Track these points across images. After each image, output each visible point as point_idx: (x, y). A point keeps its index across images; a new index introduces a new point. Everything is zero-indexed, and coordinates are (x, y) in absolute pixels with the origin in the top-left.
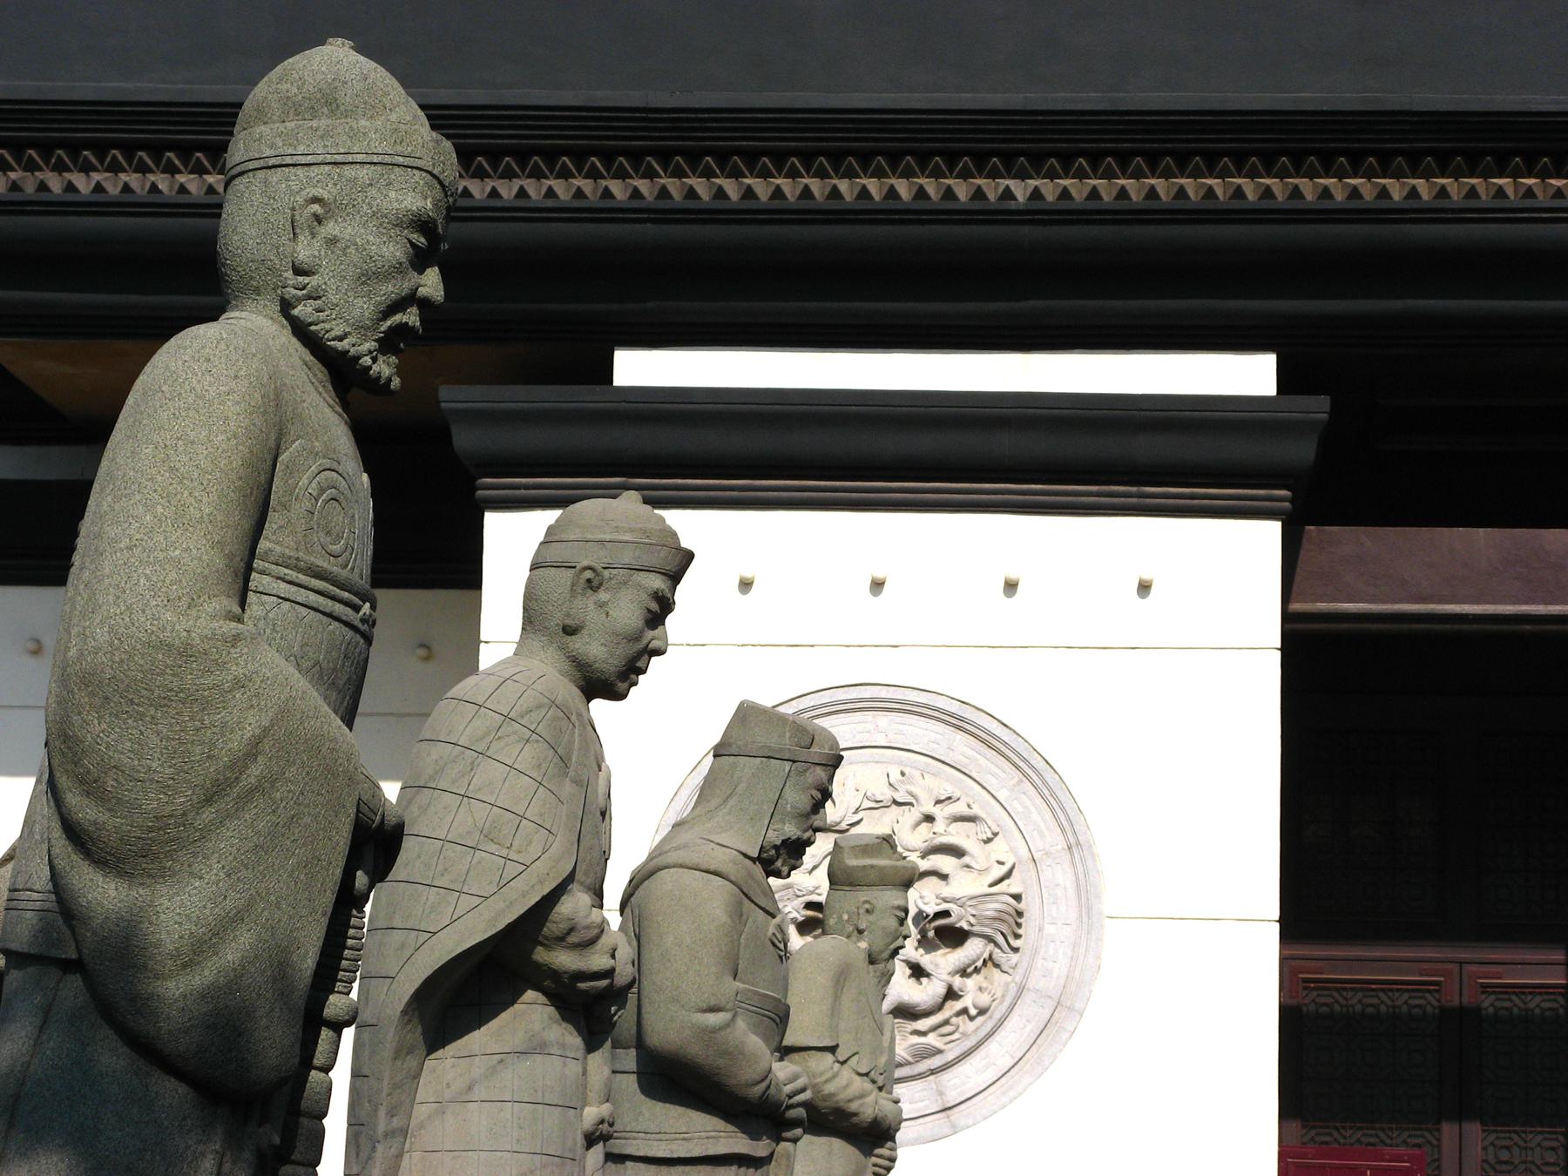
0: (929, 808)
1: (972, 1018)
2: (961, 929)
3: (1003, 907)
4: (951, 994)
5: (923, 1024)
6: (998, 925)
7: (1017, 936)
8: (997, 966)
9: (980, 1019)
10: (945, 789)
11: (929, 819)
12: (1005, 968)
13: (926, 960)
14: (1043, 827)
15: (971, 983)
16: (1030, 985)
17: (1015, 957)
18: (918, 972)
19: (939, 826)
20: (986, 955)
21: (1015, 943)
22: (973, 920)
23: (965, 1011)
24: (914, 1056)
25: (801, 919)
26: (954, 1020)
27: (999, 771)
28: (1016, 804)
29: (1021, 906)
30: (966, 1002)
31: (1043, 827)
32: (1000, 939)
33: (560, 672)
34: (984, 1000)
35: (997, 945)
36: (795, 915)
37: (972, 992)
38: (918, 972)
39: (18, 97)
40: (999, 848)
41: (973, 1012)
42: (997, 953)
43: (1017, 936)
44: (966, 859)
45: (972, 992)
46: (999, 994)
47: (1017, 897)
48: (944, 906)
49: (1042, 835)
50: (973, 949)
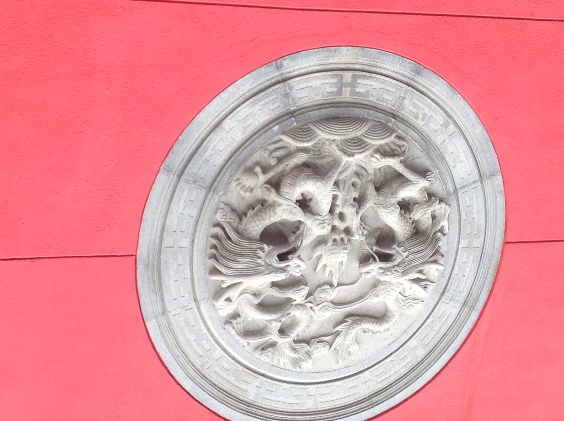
0: (282, 341)
1: (257, 164)
2: (268, 244)
3: (231, 264)
4: (276, 185)
5: (301, 158)
6: (236, 249)
7: (216, 237)
8: (233, 210)
9: (249, 163)
10: (265, 357)
11: (282, 332)
12: (227, 209)
13: (298, 215)
14: (186, 330)
15: (259, 193)
16: (204, 192)
17: (219, 217)
18: (304, 204)
19: (276, 326)
20: (245, 220)
21: (218, 230)
22: (260, 253)
23: (265, 170)
24: (309, 130)
25: (395, 246)
26: (273, 162)
27: (220, 372)
28: (207, 346)
29: (212, 262)
30: (262, 178)
31: (186, 330)
32: (232, 235)
33: (319, 280)
34: (249, 181)
35: (237, 231)
36: (400, 250)
37: (255, 185)
38: (304, 204)
39: (167, 366)
40: (224, 309)
41: (258, 169)
42: (235, 220)
43: (216, 237)
44: (257, 301)
45: (255, 185)
46: (234, 184)
47: (215, 271)
48: (283, 265)
49: (187, 322)
50: (256, 227)
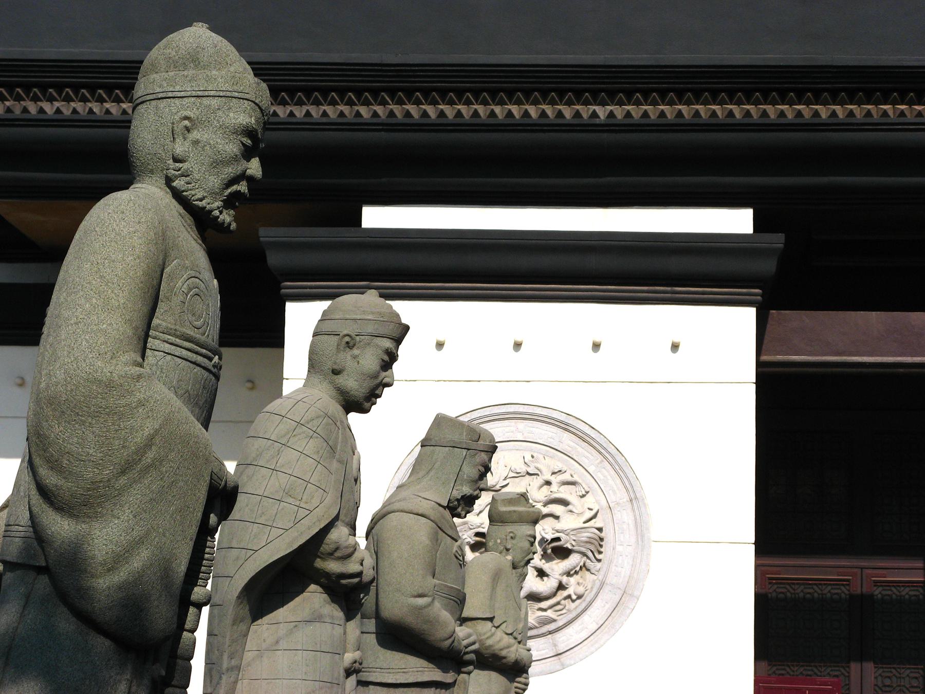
0: (548, 477)
1: (573, 601)
2: (567, 548)
3: (592, 535)
4: (561, 587)
5: (544, 604)
6: (589, 546)
7: (600, 553)
8: (588, 570)
9: (578, 601)
10: (558, 466)
11: (548, 483)
12: (593, 571)
13: (546, 566)
14: (615, 488)
15: (573, 580)
16: (608, 581)
17: (599, 565)
18: (541, 574)
19: (554, 487)
20: (582, 564)
21: (599, 557)
22: (574, 543)
23: (569, 597)
24: (539, 623)
25: (472, 542)
26: (563, 602)
27: (589, 455)
28: (599, 475)
29: (602, 535)
30: (570, 591)
31: (615, 488)
32: (590, 554)
33: (331, 397)
34: (580, 590)
35: (588, 558)
36: (469, 540)
37: (574, 586)
38: (541, 574)
40: (590, 501)
41: (574, 597)
42: (588, 563)
43: (600, 553)
44: (570, 507)
45: (574, 586)
46: (589, 587)
47: (600, 530)
48: (557, 535)
49: (615, 493)
50: (574, 560)
